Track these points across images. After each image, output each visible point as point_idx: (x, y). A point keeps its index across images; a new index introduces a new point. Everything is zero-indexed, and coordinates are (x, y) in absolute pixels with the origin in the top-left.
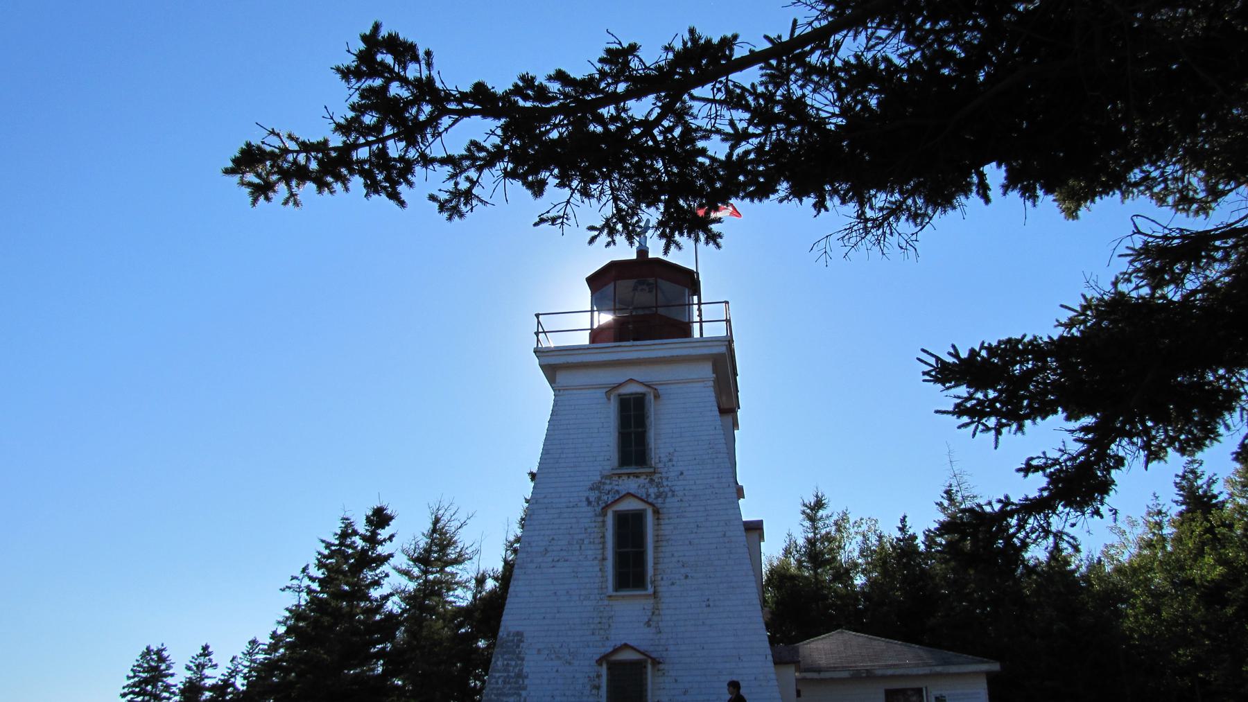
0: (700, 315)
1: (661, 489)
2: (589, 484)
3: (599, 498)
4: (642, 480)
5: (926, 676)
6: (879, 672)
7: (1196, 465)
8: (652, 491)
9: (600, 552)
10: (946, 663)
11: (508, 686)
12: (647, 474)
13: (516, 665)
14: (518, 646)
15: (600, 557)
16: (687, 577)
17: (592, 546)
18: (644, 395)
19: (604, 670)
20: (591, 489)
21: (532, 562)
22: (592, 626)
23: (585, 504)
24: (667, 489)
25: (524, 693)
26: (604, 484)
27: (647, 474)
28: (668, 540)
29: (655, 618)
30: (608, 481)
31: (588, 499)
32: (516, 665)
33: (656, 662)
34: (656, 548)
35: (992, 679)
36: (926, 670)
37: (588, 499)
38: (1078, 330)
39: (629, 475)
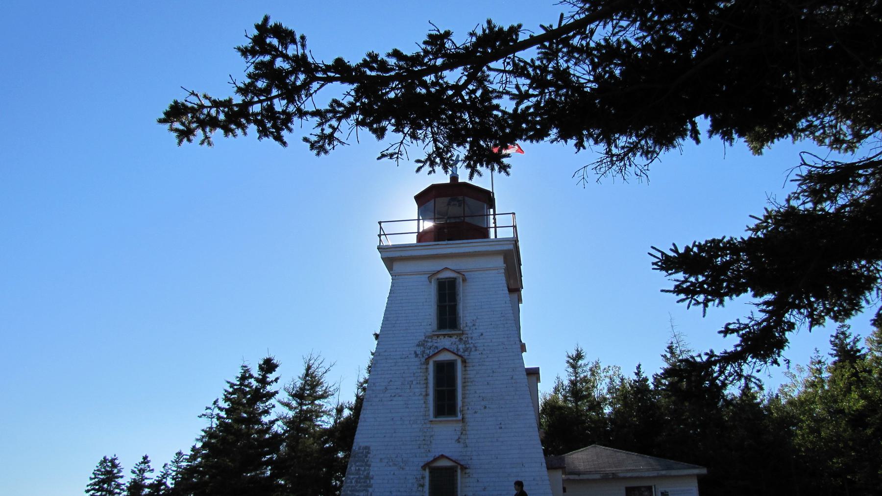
1: (468, 346)
2: (417, 342)
3: (424, 352)
4: (454, 339)
5: (654, 477)
6: (621, 475)
7: (845, 329)
8: (461, 346)
9: (424, 390)
10: (669, 468)
11: (359, 485)
12: (457, 335)
13: (365, 470)
14: (366, 457)
15: (424, 393)
16: (485, 407)
17: (418, 386)
18: (455, 279)
19: (427, 473)
20: (418, 345)
21: (376, 397)
22: (419, 442)
23: (413, 356)
24: (471, 346)
25: (370, 490)
26: (427, 342)
27: (457, 335)
28: (472, 382)
29: (463, 437)
30: (430, 340)
31: (415, 352)
32: (365, 470)
33: (464, 468)
34: (464, 387)
35: (701, 480)
36: (655, 474)
37: (415, 352)
39: (444, 335)
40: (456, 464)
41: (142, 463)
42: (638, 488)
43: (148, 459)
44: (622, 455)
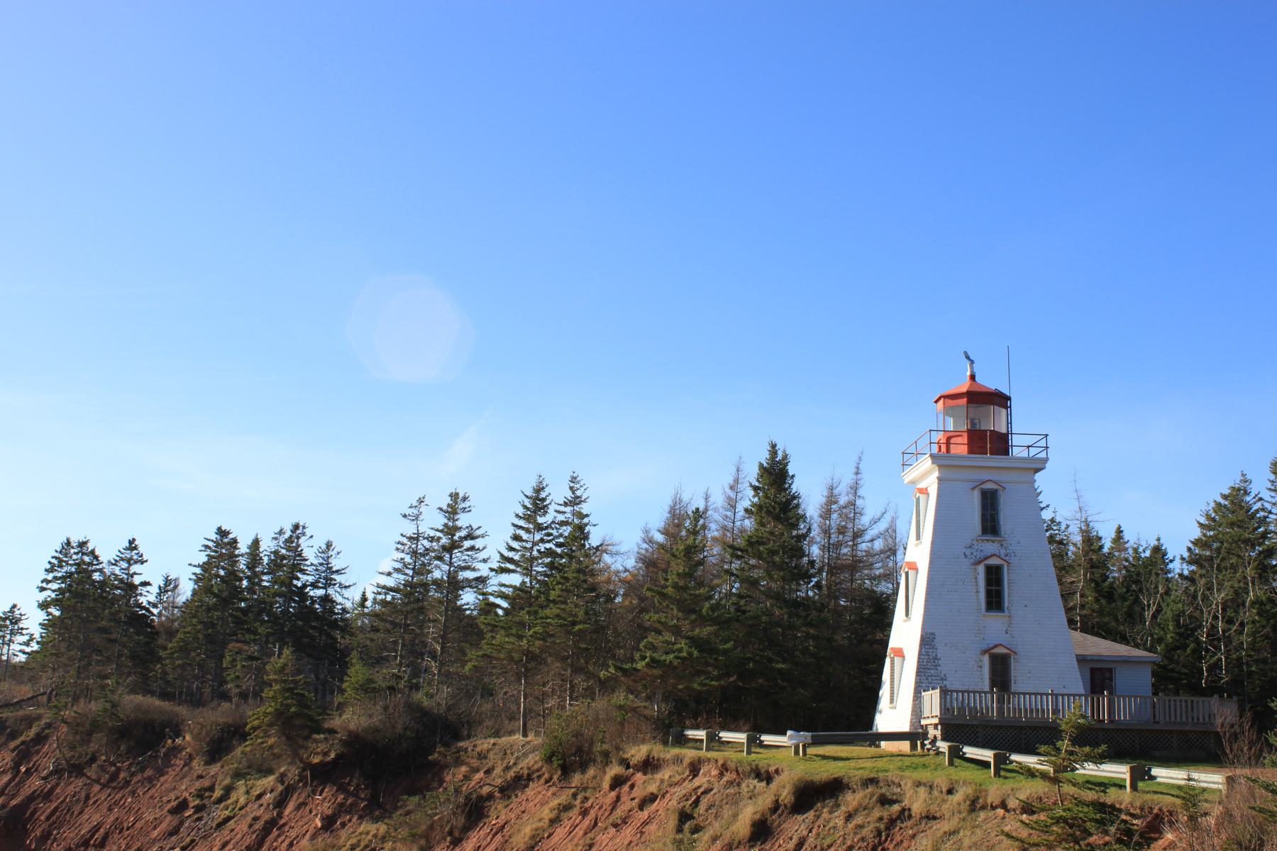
0: (940, 447)
8: (1003, 551)
12: (999, 541)
18: (996, 490)
19: (986, 659)
23: (963, 556)
27: (999, 541)
34: (1009, 587)
38: (363, 790)
39: (988, 541)
40: (1008, 651)
41: (126, 549)
42: (1101, 670)
43: (136, 543)
44: (1091, 639)
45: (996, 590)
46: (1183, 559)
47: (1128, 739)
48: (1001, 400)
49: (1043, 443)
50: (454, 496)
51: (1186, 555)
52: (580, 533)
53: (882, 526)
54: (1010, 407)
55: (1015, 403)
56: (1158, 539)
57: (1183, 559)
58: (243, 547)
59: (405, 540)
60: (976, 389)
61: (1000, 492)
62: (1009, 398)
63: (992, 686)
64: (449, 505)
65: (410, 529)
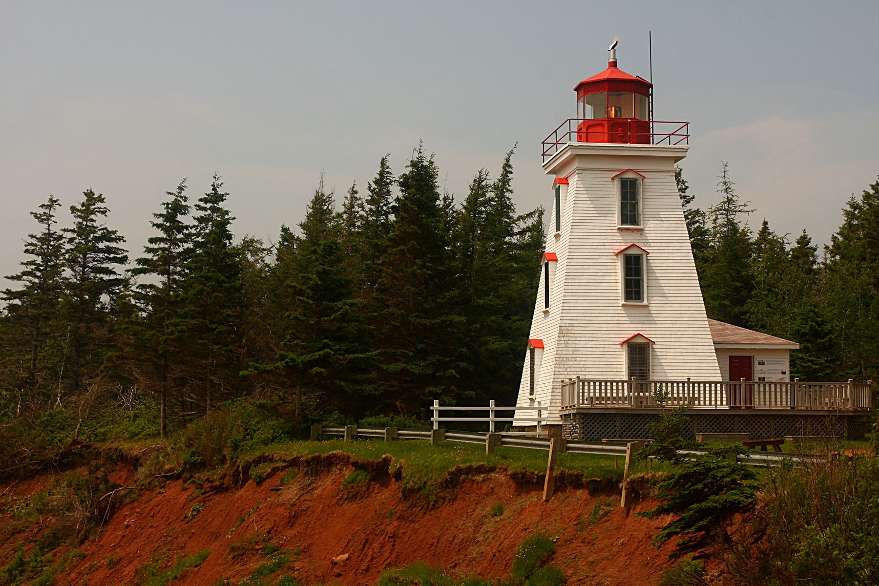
18: (636, 179)
40: (648, 341)
45: (635, 280)
46: (827, 248)
47: (764, 424)
48: (642, 88)
49: (684, 131)
50: (89, 195)
51: (830, 244)
52: (221, 231)
53: (530, 222)
54: (652, 95)
55: (655, 91)
56: (804, 231)
57: (827, 248)
58: (206, 196)
59: (34, 241)
60: (614, 76)
61: (640, 181)
62: (651, 86)
63: (630, 376)
64: (83, 205)
65: (40, 229)
